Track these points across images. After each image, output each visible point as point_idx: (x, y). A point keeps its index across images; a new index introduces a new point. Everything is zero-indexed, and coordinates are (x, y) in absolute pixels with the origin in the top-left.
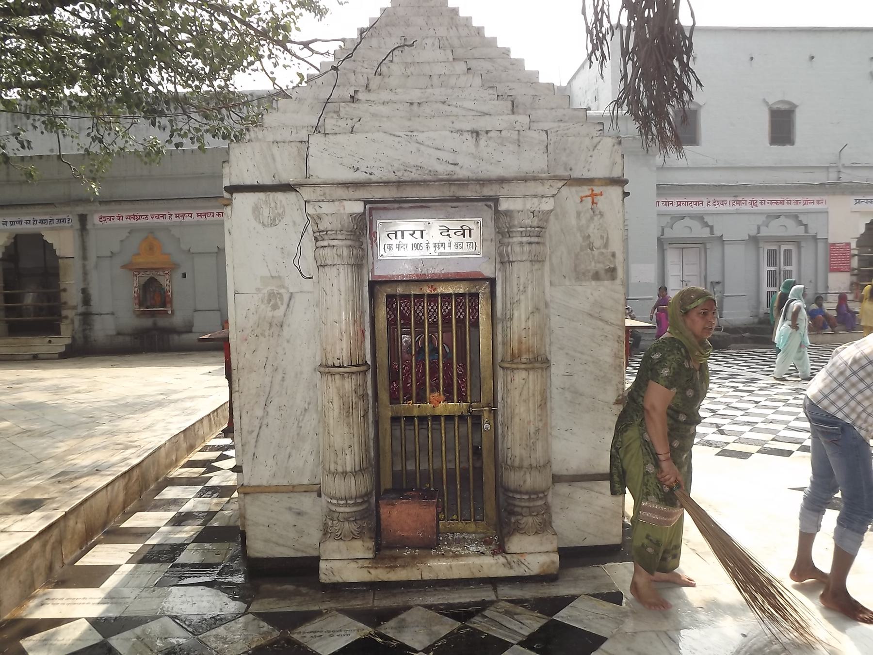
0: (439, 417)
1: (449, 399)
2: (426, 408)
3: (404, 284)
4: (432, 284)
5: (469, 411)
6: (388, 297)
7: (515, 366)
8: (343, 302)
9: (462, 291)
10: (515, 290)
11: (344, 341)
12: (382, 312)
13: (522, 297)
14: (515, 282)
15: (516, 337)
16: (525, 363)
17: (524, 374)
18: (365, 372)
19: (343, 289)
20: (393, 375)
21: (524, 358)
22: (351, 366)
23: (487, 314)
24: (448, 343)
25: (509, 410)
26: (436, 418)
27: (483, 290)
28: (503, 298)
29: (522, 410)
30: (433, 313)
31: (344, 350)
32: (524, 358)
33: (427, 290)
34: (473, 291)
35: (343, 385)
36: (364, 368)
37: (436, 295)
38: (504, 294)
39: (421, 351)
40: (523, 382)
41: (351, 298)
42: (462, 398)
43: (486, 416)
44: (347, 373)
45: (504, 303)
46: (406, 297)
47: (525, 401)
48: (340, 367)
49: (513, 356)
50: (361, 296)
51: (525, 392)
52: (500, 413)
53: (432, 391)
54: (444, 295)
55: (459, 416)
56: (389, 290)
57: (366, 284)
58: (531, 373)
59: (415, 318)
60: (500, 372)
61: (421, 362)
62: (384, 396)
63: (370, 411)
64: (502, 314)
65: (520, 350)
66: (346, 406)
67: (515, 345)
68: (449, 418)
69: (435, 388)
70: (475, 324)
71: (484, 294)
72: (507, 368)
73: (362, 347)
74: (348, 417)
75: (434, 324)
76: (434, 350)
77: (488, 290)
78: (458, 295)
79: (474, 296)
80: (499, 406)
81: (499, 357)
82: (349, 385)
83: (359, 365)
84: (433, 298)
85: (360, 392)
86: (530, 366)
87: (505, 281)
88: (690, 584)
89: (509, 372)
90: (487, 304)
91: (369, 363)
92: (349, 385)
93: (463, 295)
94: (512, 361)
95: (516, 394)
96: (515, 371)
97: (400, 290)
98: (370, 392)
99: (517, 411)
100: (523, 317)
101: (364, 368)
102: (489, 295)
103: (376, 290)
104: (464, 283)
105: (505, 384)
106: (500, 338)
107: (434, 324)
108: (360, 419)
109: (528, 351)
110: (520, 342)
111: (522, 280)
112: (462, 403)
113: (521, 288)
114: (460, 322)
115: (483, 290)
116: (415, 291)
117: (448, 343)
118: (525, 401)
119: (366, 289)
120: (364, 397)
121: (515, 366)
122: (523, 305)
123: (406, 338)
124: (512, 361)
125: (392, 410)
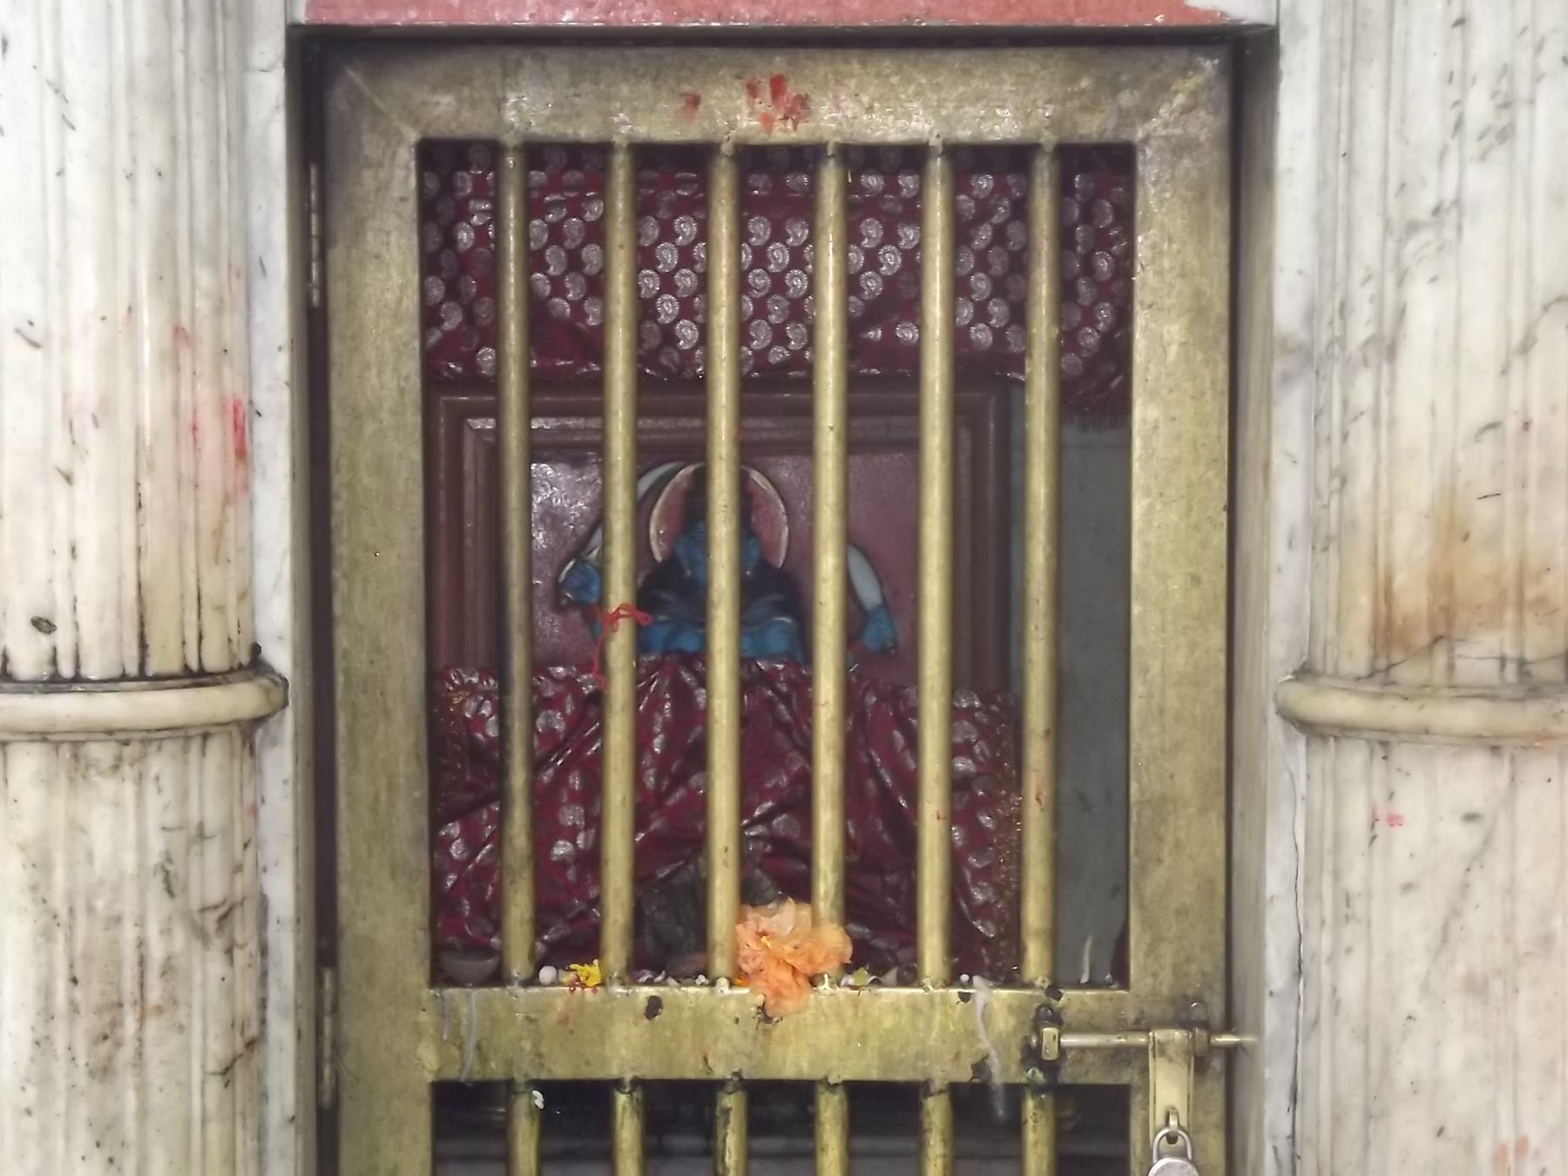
0: (802, 1093)
1: (881, 943)
2: (703, 1020)
3: (559, 63)
4: (779, 62)
5: (1032, 1055)
6: (442, 159)
7: (1401, 713)
8: (83, 189)
9: (1003, 126)
10: (1429, 121)
11: (88, 474)
12: (387, 277)
13: (1483, 181)
14: (1426, 63)
15: (1418, 488)
16: (1489, 695)
17: (1472, 781)
18: (248, 733)
19: (83, 79)
20: (460, 774)
21: (1479, 655)
22: (144, 677)
23: (1198, 312)
24: (883, 542)
25: (1352, 1053)
26: (781, 1107)
27: (1171, 121)
28: (1322, 185)
29: (1452, 1058)
30: (778, 306)
31: (89, 551)
32: (1479, 655)
33: (736, 114)
34: (1093, 127)
35: (77, 829)
36: (242, 699)
37: (806, 157)
38: (1340, 152)
39: (671, 588)
40: (1464, 838)
41: (153, 152)
42: (981, 951)
43: (1168, 1090)
44: (43, 736)
45: (1333, 227)
46: (570, 166)
47: (1475, 987)
48: (54, 683)
49: (1388, 634)
50: (234, 139)
51: (1480, 919)
52: (1274, 1076)
53: (749, 895)
54: (862, 157)
55: (956, 1092)
56: (447, 109)
57: (270, 50)
58: (1537, 769)
59: (643, 358)
60: (1285, 765)
61: (673, 669)
62: (389, 916)
63: (282, 1033)
64: (1311, 315)
65: (1443, 585)
66: (89, 995)
67: (1410, 548)
68: (882, 1107)
69: (778, 871)
70: (1099, 392)
71: (1181, 148)
72: (1342, 731)
73: (225, 542)
74: (103, 1072)
75: (776, 388)
76: (776, 588)
77: (1208, 125)
78: (970, 159)
79: (1100, 175)
80: (1273, 1018)
81: (1275, 645)
82: (119, 827)
83: (196, 677)
84: (776, 180)
85: (209, 881)
86: (1527, 717)
87: (1347, 56)
88: (980, 1067)
89: (1355, 758)
90: (1199, 228)
91: (281, 657)
92: (119, 827)
93: (1011, 159)
94: (1380, 677)
95: (1407, 927)
96: (1403, 756)
97: (528, 108)
98: (283, 889)
99: (1410, 1063)
100: (1483, 337)
101: (242, 699)
102: (1213, 161)
103: (339, 101)
104: (1031, 62)
105: (1324, 853)
106: (1287, 496)
107: (776, 388)
108: (207, 1097)
109: (1520, 596)
110: (1452, 530)
111: (1487, 46)
112: (984, 992)
113: (1479, 107)
114: (986, 376)
115: (1171, 121)
116: (642, 115)
117: (883, 542)
118: (1475, 987)
119: (270, 89)
120: (225, 921)
121: (1401, 713)
122: (1481, 240)
123: (556, 486)
124: (1380, 677)
125: (450, 1033)
